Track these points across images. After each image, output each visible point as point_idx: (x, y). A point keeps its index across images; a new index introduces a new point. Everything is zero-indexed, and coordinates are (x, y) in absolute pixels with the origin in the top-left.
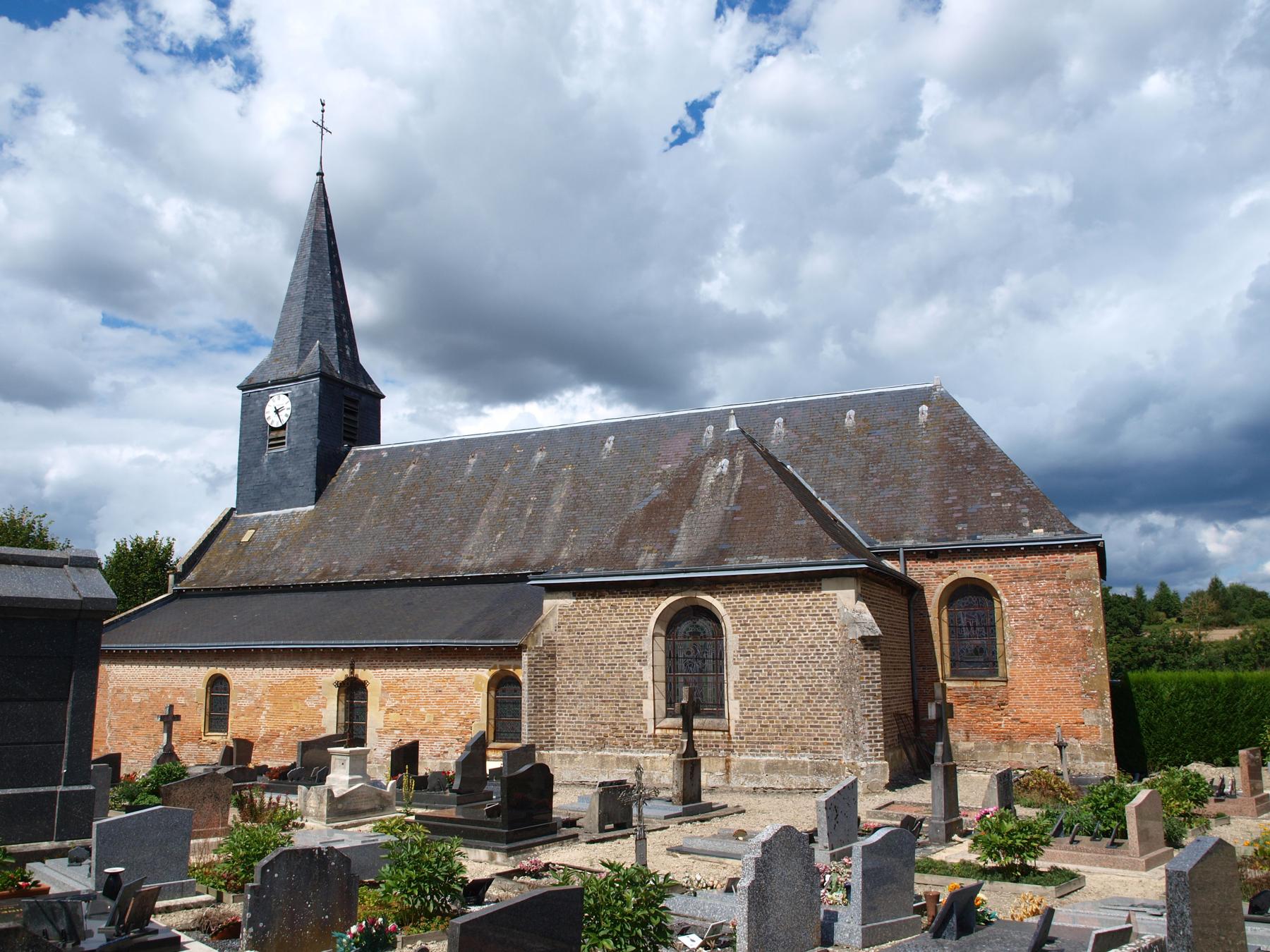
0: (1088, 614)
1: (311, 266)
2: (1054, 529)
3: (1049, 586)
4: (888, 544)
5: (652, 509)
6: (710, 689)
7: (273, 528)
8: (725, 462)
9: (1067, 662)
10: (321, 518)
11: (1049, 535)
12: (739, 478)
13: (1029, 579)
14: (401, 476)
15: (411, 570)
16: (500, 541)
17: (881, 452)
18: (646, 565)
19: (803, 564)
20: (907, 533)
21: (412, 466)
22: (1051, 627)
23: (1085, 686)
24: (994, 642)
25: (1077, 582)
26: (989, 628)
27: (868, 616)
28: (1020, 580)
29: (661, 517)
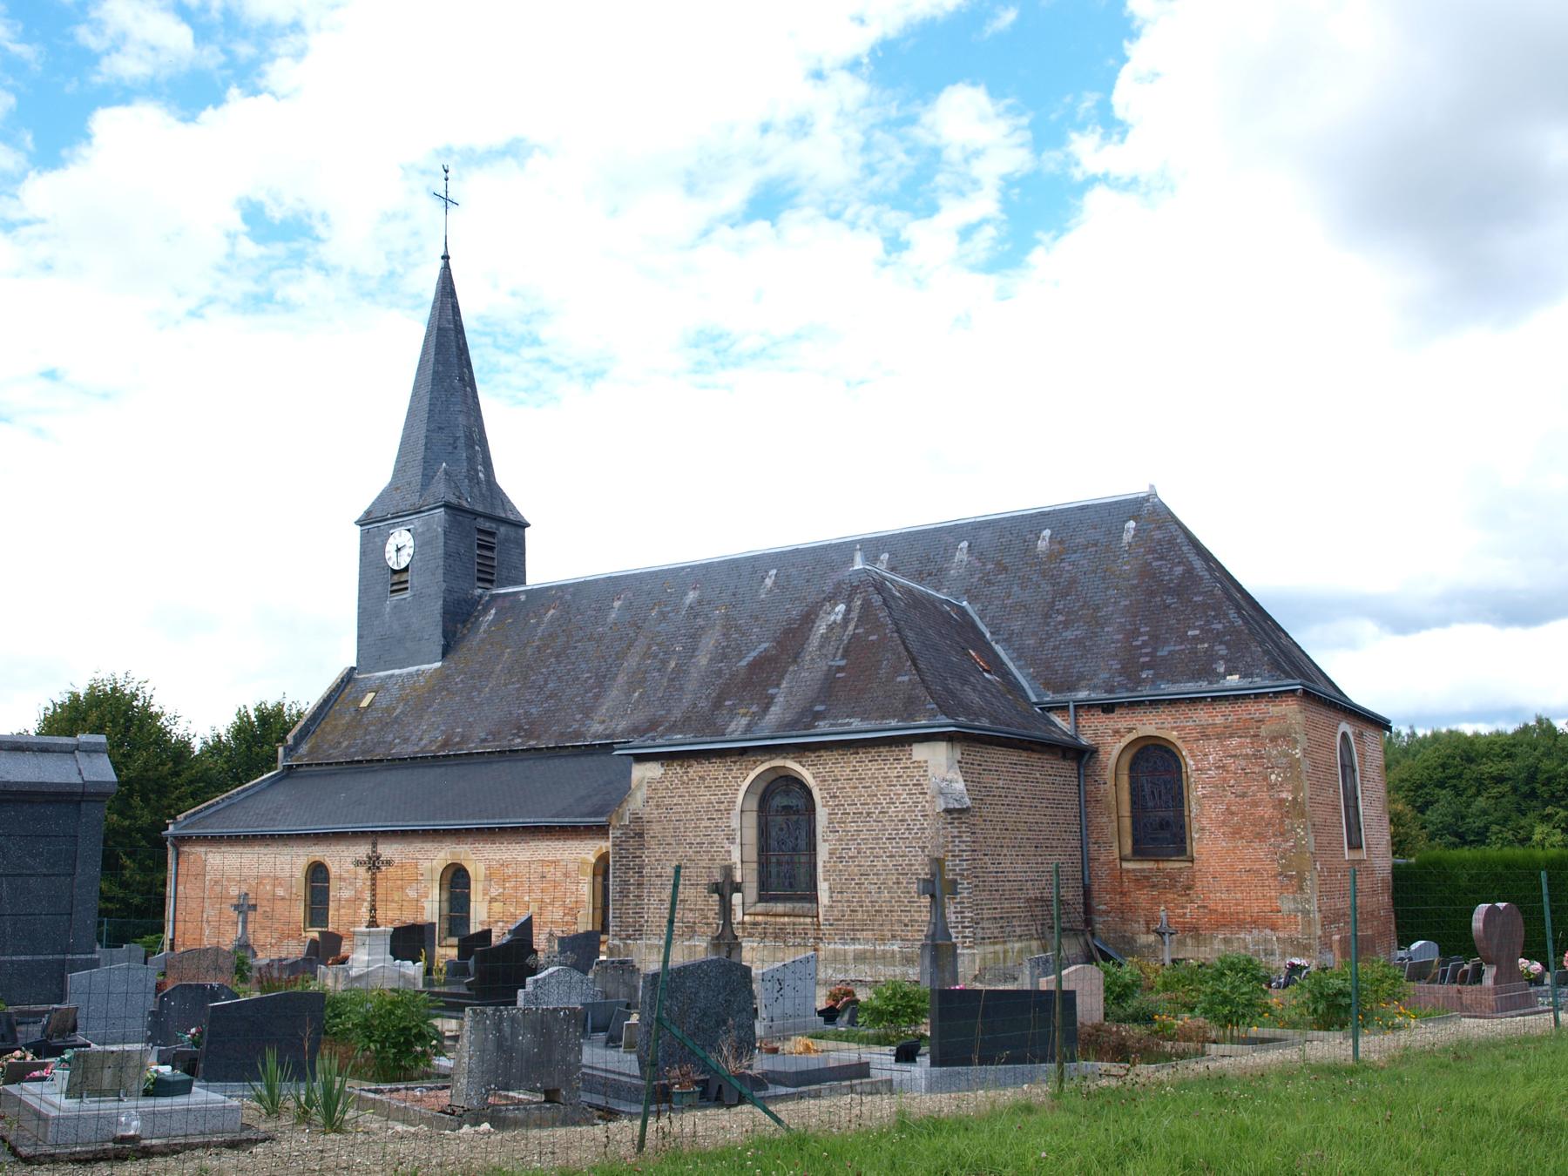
0: (1286, 779)
1: (435, 372)
2: (1251, 675)
3: (1241, 746)
4: (1059, 697)
5: (755, 666)
6: (802, 870)
7: (395, 691)
8: (841, 608)
9: (1261, 837)
10: (447, 676)
11: (1245, 683)
12: (851, 627)
13: (1220, 737)
14: (538, 624)
15: (538, 738)
16: (637, 701)
17: (1073, 581)
18: (736, 730)
19: (893, 726)
20: (1083, 683)
21: (552, 612)
22: (1244, 795)
23: (1283, 866)
24: (1182, 815)
25: (1273, 739)
26: (1177, 797)
27: (960, 786)
28: (1208, 737)
29: (758, 679)
